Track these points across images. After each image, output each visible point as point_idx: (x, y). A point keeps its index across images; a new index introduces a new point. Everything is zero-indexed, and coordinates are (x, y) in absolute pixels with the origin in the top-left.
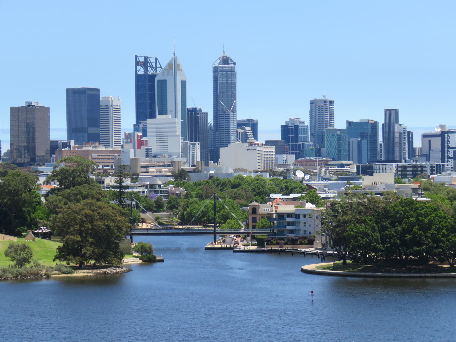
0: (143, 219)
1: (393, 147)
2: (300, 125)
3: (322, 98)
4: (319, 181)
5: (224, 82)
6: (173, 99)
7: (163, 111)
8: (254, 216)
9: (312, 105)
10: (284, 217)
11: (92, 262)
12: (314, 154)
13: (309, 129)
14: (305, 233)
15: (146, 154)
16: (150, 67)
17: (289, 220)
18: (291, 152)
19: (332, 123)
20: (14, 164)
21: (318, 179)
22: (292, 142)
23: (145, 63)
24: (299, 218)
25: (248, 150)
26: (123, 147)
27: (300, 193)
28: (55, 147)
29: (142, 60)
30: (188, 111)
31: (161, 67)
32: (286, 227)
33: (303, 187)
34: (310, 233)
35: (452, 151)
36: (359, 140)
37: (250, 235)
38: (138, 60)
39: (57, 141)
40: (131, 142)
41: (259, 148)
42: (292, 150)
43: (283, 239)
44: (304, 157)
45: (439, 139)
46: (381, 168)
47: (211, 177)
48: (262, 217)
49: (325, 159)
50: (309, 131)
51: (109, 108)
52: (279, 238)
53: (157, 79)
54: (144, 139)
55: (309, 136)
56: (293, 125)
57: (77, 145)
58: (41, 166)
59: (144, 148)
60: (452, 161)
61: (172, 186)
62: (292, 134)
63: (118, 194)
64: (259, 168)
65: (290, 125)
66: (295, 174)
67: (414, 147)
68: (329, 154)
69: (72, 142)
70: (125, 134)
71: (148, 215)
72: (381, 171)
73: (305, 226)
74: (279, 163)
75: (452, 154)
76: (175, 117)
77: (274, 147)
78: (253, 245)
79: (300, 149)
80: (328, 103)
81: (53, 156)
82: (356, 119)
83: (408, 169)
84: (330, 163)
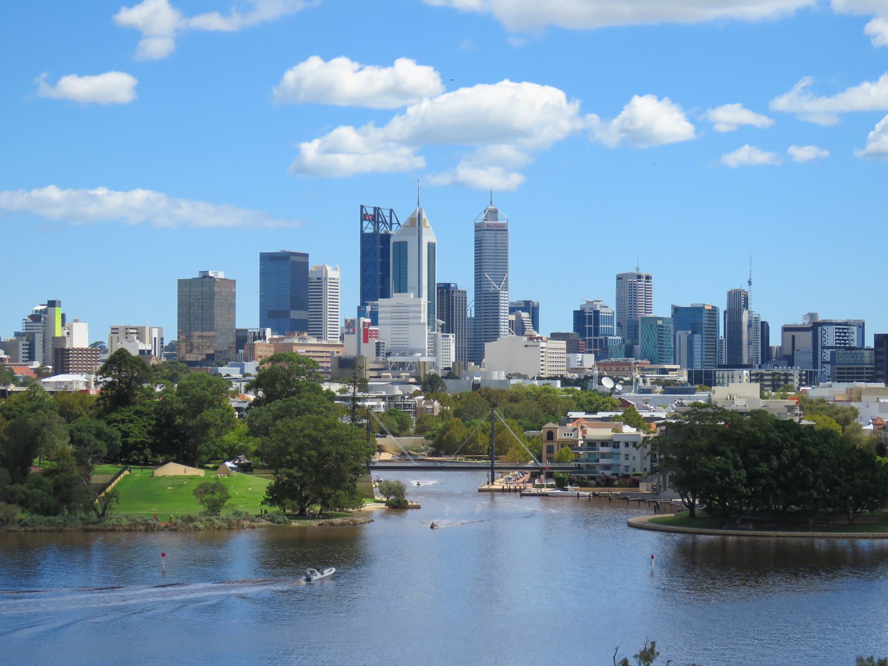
0: (379, 446)
1: (740, 343)
2: (602, 310)
3: (635, 271)
5: (490, 245)
6: (419, 272)
7: (402, 288)
8: (550, 444)
11: (318, 508)
14: (627, 470)
16: (382, 222)
17: (603, 450)
18: (587, 350)
19: (648, 308)
20: (182, 362)
22: (590, 335)
23: (375, 217)
24: (618, 447)
25: (526, 346)
26: (342, 338)
27: (611, 411)
28: (242, 340)
29: (371, 212)
31: (398, 223)
32: (598, 461)
34: (634, 470)
35: (828, 352)
36: (690, 332)
37: (544, 471)
38: (364, 212)
39: (246, 330)
40: (354, 333)
41: (542, 344)
42: (590, 347)
43: (593, 478)
45: (809, 334)
46: (726, 376)
47: (476, 386)
48: (562, 446)
49: (639, 361)
53: (392, 241)
57: (275, 337)
58: (222, 366)
60: (828, 367)
61: (422, 397)
62: (590, 323)
63: (349, 408)
66: (600, 384)
67: (771, 345)
68: (645, 354)
69: (268, 331)
71: (388, 441)
72: (726, 380)
75: (829, 356)
78: (548, 487)
79: (601, 346)
80: (644, 279)
81: (241, 351)
82: (685, 303)
83: (765, 378)
84: (646, 367)
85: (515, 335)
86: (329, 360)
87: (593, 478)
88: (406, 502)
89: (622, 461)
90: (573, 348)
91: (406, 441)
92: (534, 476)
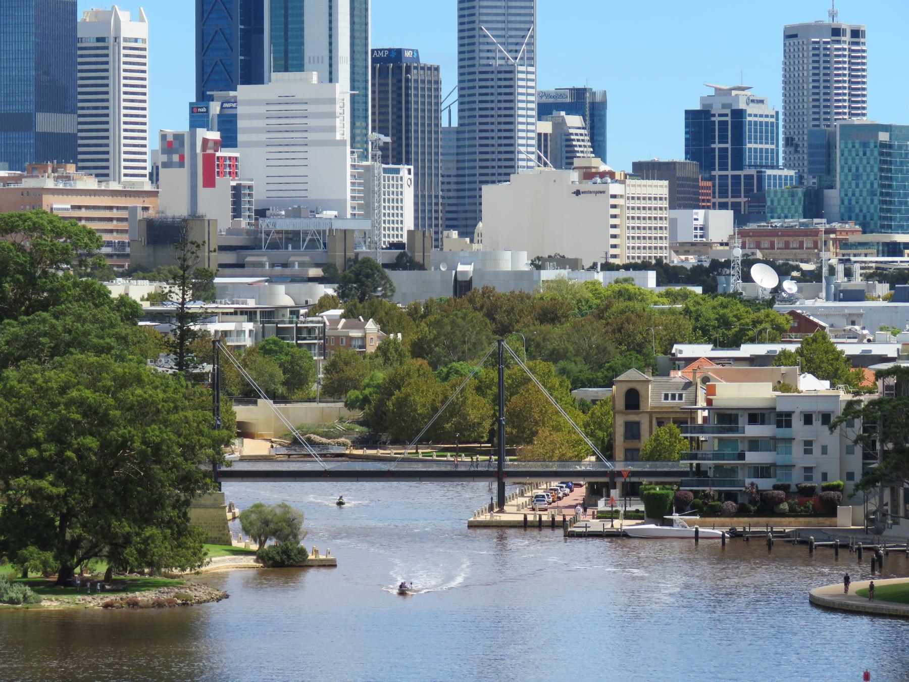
0: (241, 425)
2: (751, 109)
3: (827, 20)
4: (827, 299)
7: (291, 60)
9: (791, 41)
10: (737, 422)
11: (101, 568)
12: (800, 210)
13: (781, 123)
14: (808, 478)
15: (234, 203)
18: (717, 200)
19: (857, 105)
21: (823, 294)
22: (723, 167)
24: (789, 424)
25: (578, 193)
30: (374, 60)
32: (742, 456)
33: (781, 320)
34: (825, 476)
40: (181, 164)
41: (614, 188)
42: (723, 194)
43: (730, 496)
44: (765, 220)
47: (462, 286)
48: (660, 423)
50: (781, 130)
51: (107, 48)
52: (720, 493)
54: (223, 153)
55: (781, 149)
56: (728, 111)
59: (225, 184)
61: (339, 312)
63: (172, 338)
64: (614, 256)
65: (717, 109)
68: (850, 209)
70: (164, 137)
73: (808, 452)
74: (680, 240)
76: (331, 80)
77: (666, 183)
79: (749, 191)
80: (847, 38)
84: (852, 238)
85: (551, 169)
86: (124, 226)
87: (730, 496)
88: (302, 552)
89: (797, 456)
90: (684, 196)
91: (302, 413)
92: (596, 492)
